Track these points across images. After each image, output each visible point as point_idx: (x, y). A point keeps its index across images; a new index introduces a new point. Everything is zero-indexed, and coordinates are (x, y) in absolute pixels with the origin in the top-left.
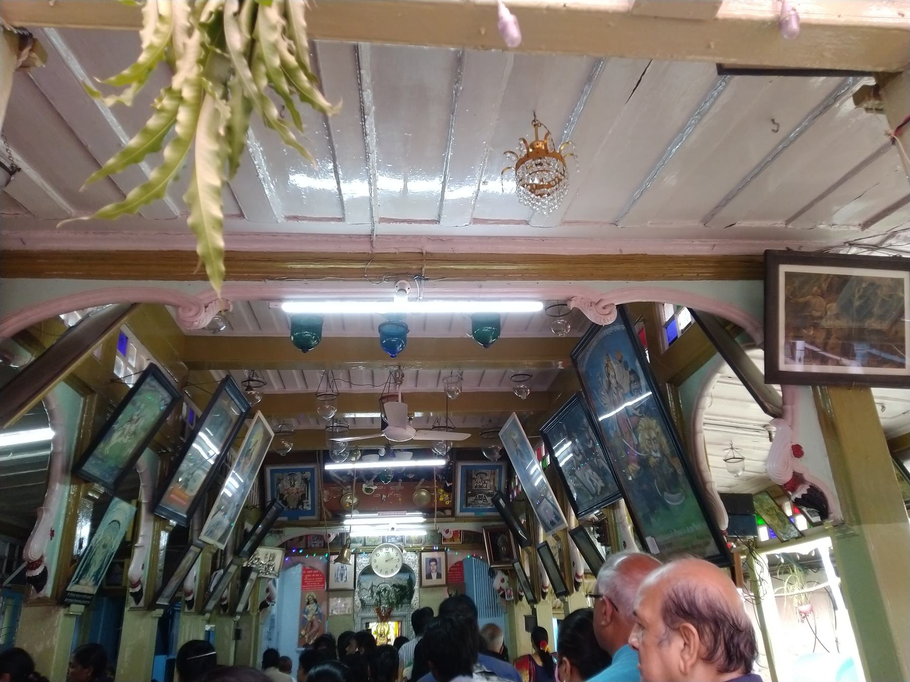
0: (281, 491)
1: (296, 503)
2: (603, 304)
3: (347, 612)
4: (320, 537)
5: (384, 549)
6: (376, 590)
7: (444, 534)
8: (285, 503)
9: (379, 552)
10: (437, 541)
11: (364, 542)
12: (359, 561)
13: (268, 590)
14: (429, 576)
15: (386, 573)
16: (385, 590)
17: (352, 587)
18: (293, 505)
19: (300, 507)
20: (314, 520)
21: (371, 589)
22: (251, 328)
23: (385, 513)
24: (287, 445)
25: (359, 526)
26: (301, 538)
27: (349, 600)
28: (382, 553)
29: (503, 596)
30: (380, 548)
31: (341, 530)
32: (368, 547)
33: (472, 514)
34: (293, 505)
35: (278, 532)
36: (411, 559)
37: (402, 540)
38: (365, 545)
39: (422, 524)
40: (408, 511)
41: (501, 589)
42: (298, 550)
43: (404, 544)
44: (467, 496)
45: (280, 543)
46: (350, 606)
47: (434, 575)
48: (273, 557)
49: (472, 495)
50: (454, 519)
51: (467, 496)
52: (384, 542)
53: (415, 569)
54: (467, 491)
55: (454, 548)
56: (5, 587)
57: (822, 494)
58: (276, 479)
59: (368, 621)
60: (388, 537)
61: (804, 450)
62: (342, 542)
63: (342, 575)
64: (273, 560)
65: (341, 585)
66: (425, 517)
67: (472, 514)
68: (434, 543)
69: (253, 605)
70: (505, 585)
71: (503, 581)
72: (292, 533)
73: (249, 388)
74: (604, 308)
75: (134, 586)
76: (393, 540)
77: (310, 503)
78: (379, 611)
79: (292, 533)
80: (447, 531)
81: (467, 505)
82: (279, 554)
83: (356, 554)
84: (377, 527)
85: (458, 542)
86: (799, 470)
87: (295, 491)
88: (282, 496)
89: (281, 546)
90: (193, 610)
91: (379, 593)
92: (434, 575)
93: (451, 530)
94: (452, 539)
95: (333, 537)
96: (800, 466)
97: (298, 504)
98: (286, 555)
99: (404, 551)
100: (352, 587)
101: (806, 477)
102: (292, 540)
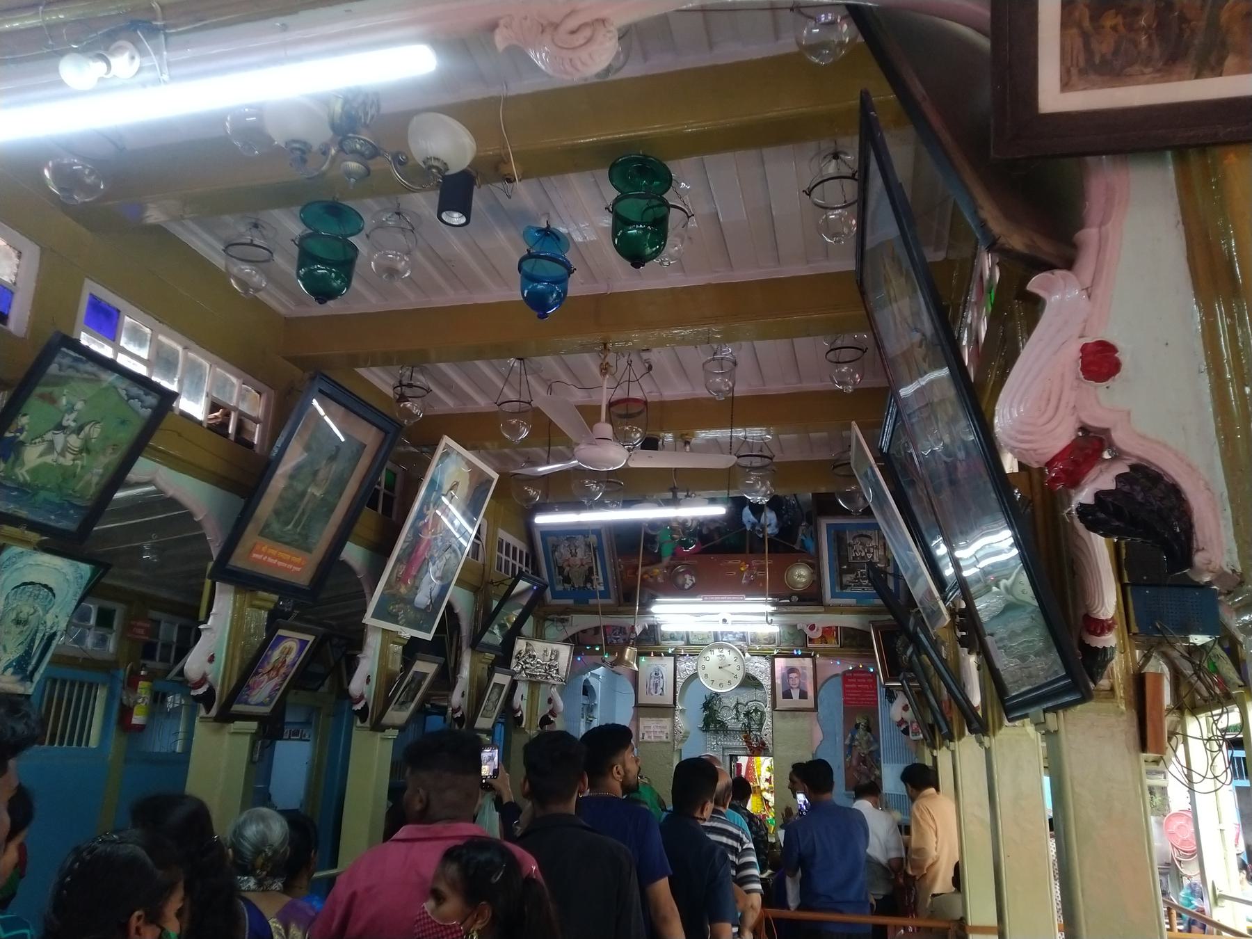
0: (560, 562)
1: (582, 580)
2: (572, 23)
3: (664, 739)
4: (622, 630)
5: (716, 651)
6: (743, 709)
7: (807, 631)
8: (567, 580)
9: (709, 654)
10: (799, 642)
11: (687, 638)
12: (681, 666)
13: (550, 701)
14: (787, 695)
15: (721, 685)
16: (756, 711)
17: (670, 702)
18: (578, 582)
19: (589, 586)
20: (610, 605)
21: (736, 707)
22: (374, 301)
23: (712, 597)
24: (532, 492)
25: (673, 615)
26: (597, 629)
27: (666, 722)
28: (714, 656)
29: (906, 732)
30: (711, 649)
31: (650, 620)
32: (693, 647)
33: (852, 601)
34: (578, 582)
35: (563, 621)
36: (759, 667)
37: (743, 639)
38: (688, 643)
39: (772, 614)
40: (748, 596)
41: (902, 721)
42: (593, 646)
43: (748, 645)
44: (841, 573)
45: (564, 636)
46: (668, 730)
47: (795, 694)
48: (556, 655)
49: (849, 571)
50: (821, 609)
51: (841, 573)
52: (717, 640)
53: (766, 682)
54: (840, 565)
55: (827, 654)
56: (171, 681)
57: (1175, 490)
58: (550, 546)
59: (735, 752)
60: (722, 633)
61: (1124, 356)
62: (650, 641)
63: (656, 685)
64: (556, 659)
65: (655, 699)
66: (773, 604)
67: (852, 601)
68: (794, 645)
69: (530, 720)
70: (909, 715)
71: (905, 708)
72: (581, 622)
73: (403, 398)
74: (573, 32)
75: (198, 685)
76: (730, 638)
77: (601, 580)
78: (747, 740)
79: (581, 622)
80: (812, 627)
81: (843, 587)
82: (565, 652)
83: (676, 655)
84: (702, 618)
85: (833, 644)
86: (1096, 420)
87: (579, 563)
88: (561, 569)
89: (566, 641)
90: (367, 724)
91: (747, 714)
92: (795, 694)
93: (819, 626)
94: (823, 639)
95: (638, 630)
96: (1103, 404)
97: (585, 583)
98: (576, 653)
99: (747, 655)
100: (670, 702)
101: (1118, 437)
102: (584, 631)
